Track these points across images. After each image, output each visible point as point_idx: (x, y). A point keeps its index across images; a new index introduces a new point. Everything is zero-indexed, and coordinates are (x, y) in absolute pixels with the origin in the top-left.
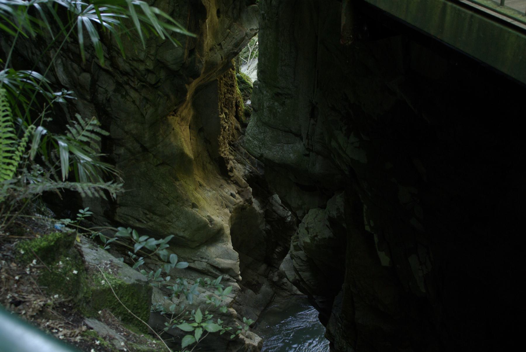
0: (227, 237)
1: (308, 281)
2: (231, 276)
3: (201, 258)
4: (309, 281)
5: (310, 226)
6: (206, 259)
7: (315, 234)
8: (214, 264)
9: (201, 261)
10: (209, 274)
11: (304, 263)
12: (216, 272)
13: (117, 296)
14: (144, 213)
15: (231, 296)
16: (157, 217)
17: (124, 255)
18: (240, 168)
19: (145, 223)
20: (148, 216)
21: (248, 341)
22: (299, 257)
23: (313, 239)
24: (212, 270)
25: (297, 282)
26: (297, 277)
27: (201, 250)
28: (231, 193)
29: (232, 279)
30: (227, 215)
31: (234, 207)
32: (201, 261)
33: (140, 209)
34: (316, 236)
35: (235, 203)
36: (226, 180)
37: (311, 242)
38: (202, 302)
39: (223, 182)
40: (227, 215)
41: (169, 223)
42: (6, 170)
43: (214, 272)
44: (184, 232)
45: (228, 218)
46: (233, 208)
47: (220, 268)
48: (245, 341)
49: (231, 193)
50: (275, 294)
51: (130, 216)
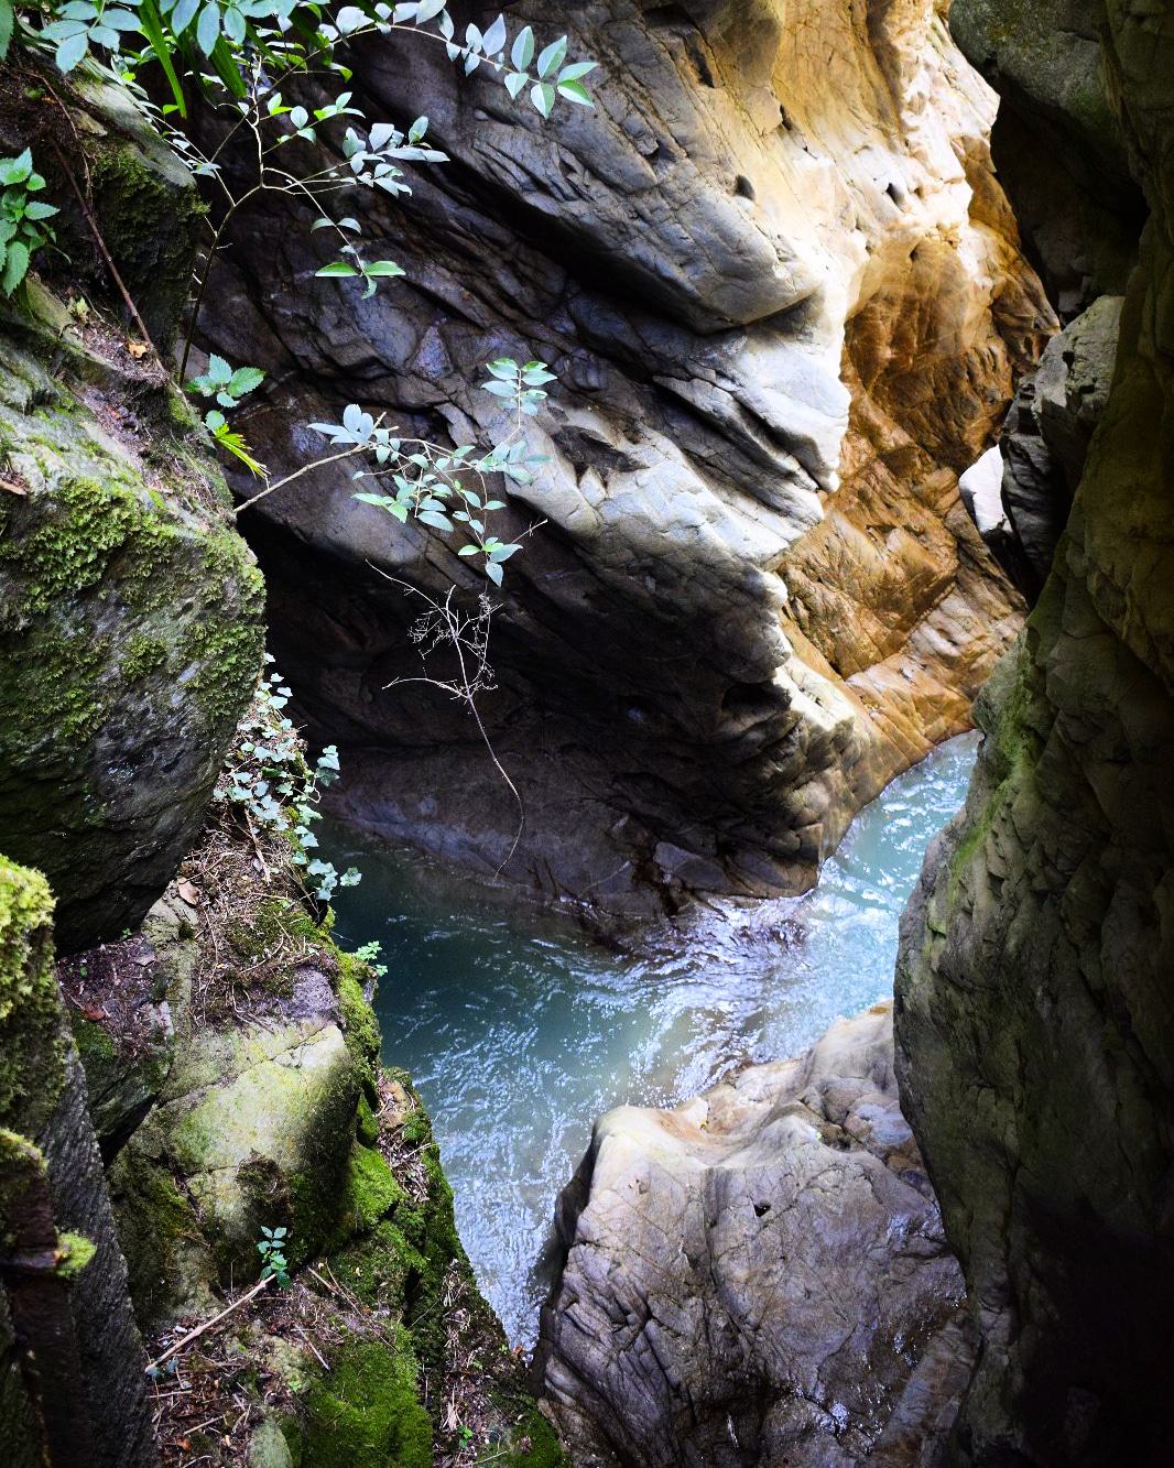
0: (828, 330)
1: (1032, 545)
2: (803, 466)
3: (718, 373)
4: (1036, 548)
5: (1079, 350)
6: (733, 380)
7: (1087, 382)
8: (756, 407)
9: (714, 385)
10: (731, 435)
11: (1037, 482)
12: (756, 434)
13: (263, 150)
14: (562, 162)
15: (782, 532)
16: (605, 190)
17: (467, 289)
18: (950, 106)
19: (556, 199)
20: (574, 178)
21: (799, 703)
22: (1027, 455)
23: (1075, 397)
24: (742, 424)
25: (1004, 542)
26: (1007, 527)
27: (725, 347)
28: (890, 185)
29: (803, 475)
30: (854, 255)
31: (887, 235)
32: (714, 385)
33: (554, 144)
34: (1090, 389)
35: (892, 224)
36: (886, 134)
37: (1068, 405)
38: (679, 522)
39: (874, 136)
40: (854, 255)
41: (638, 223)
42: (634, 90)
43: (749, 433)
44: (681, 265)
45: (853, 268)
46: (882, 239)
47: (772, 425)
48: (790, 700)
49: (890, 185)
50: (953, 585)
51: (515, 161)
